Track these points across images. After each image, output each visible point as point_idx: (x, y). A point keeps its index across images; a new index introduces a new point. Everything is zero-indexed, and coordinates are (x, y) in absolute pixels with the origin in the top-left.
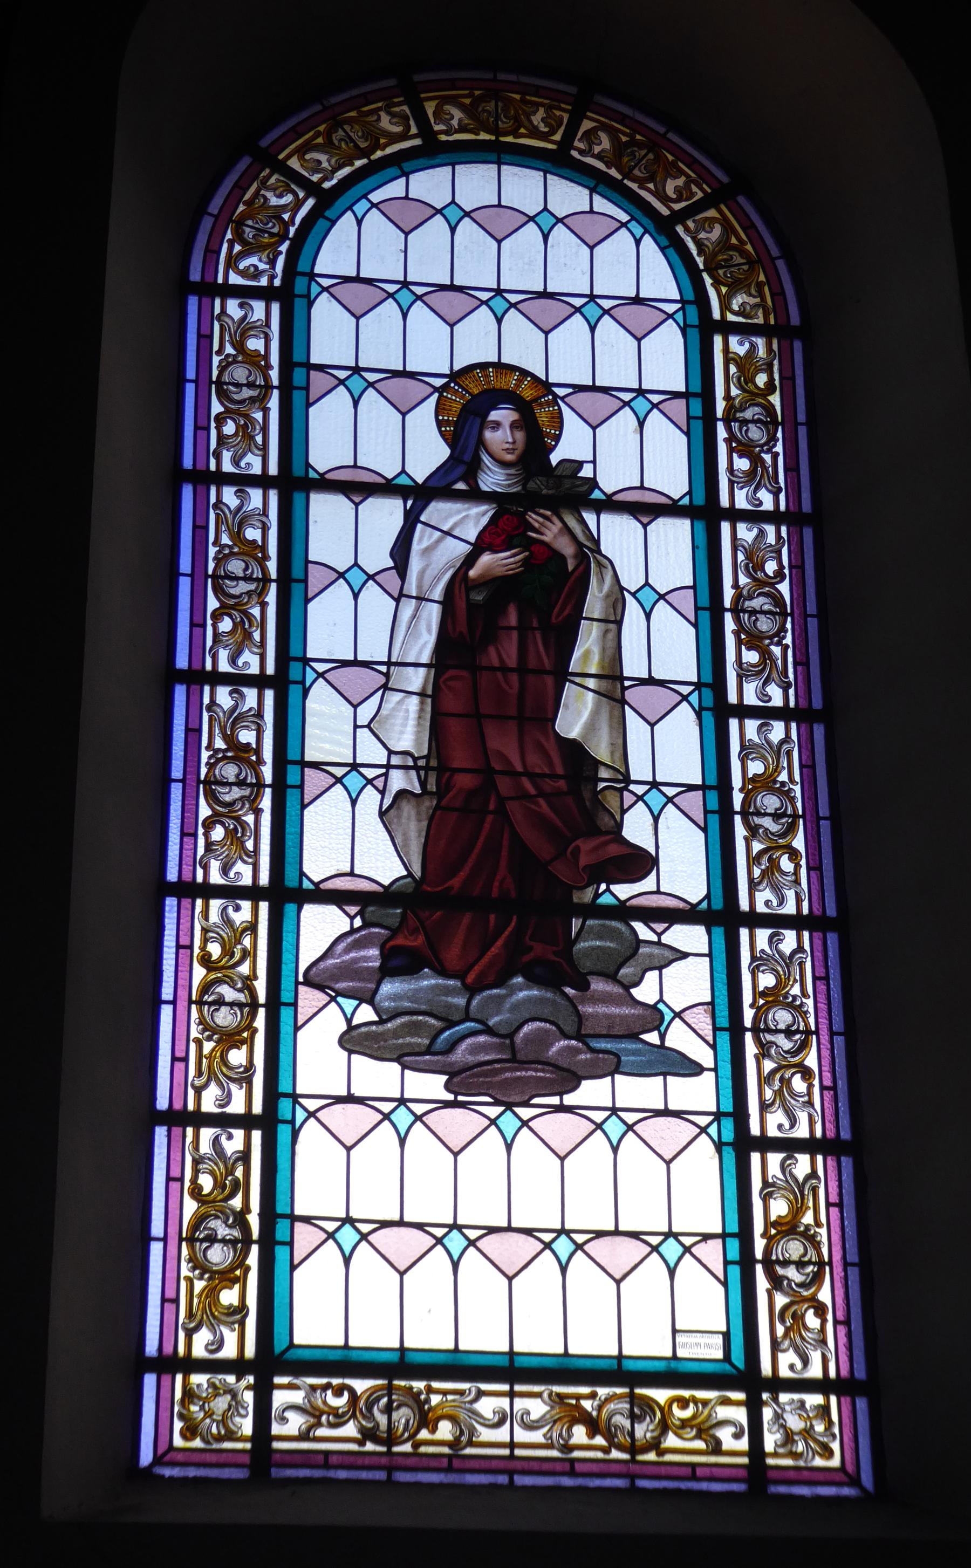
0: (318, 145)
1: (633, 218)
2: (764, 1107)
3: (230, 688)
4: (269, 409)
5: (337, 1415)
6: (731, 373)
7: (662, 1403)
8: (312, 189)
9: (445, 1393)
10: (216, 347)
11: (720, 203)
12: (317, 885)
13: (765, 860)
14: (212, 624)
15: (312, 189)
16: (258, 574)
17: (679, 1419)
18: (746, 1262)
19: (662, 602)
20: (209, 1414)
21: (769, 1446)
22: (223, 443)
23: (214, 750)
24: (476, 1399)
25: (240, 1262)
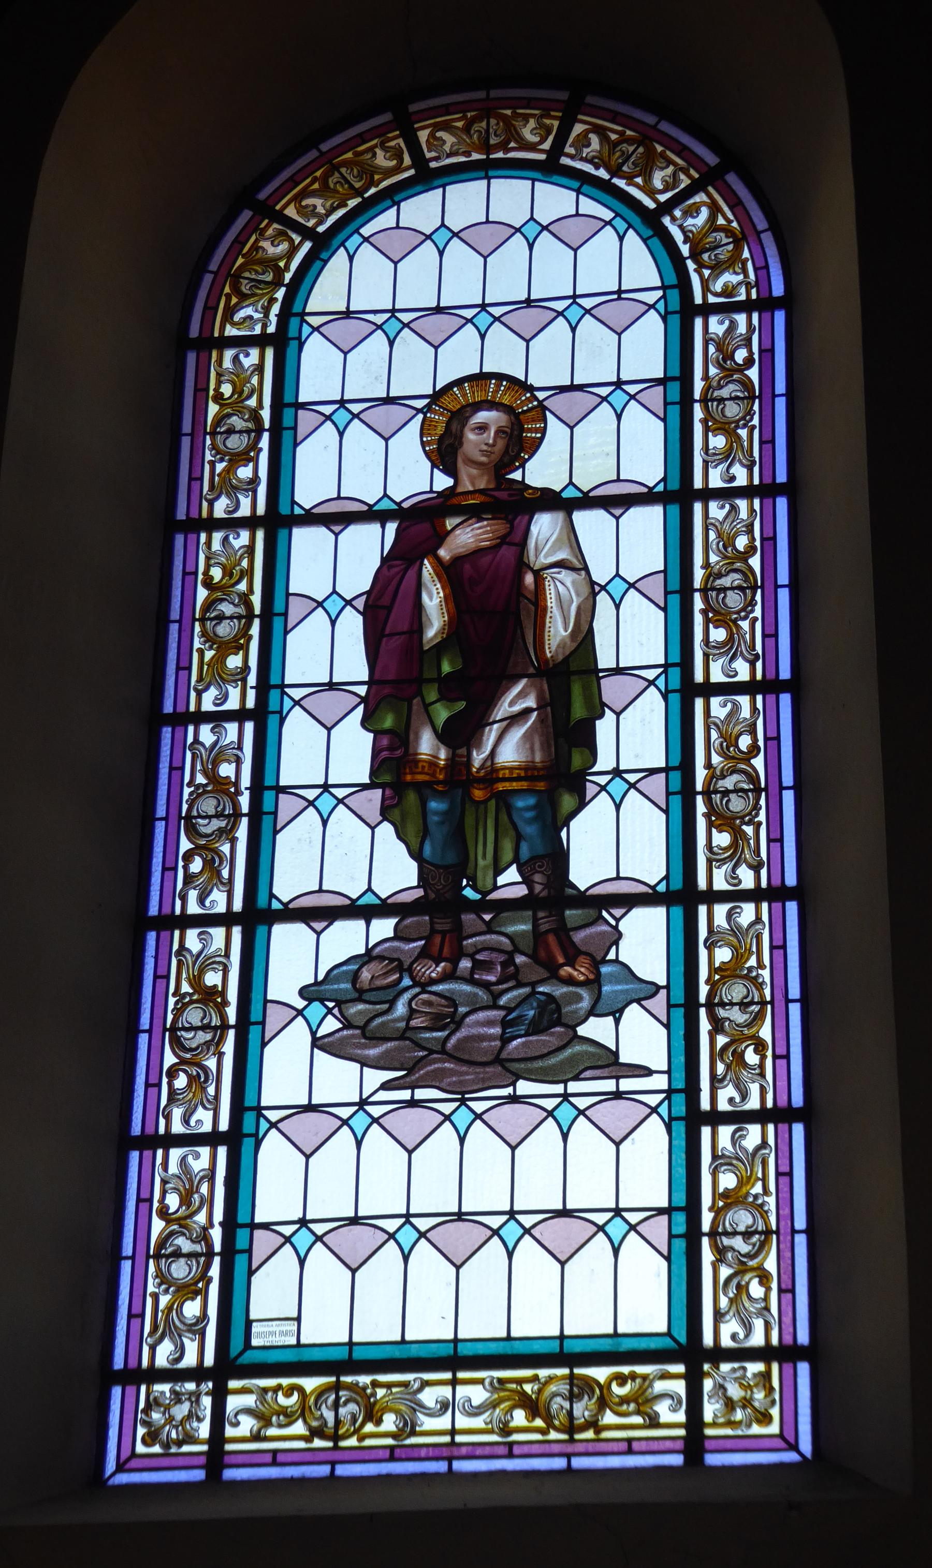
0: (315, 191)
1: (617, 215)
2: (719, 1316)
3: (211, 726)
4: (224, 1053)
5: (286, 1415)
6: (711, 540)
7: (602, 1381)
8: (307, 233)
9: (389, 1386)
10: (187, 779)
11: (707, 186)
12: (286, 905)
13: (729, 1056)
14: (183, 867)
15: (307, 233)
16: (216, 1021)
17: (618, 1396)
18: (691, 1006)
19: (632, 590)
20: (171, 1419)
21: (708, 1417)
22: (173, 1099)
23: (195, 785)
24: (420, 1389)
25: (254, 446)
